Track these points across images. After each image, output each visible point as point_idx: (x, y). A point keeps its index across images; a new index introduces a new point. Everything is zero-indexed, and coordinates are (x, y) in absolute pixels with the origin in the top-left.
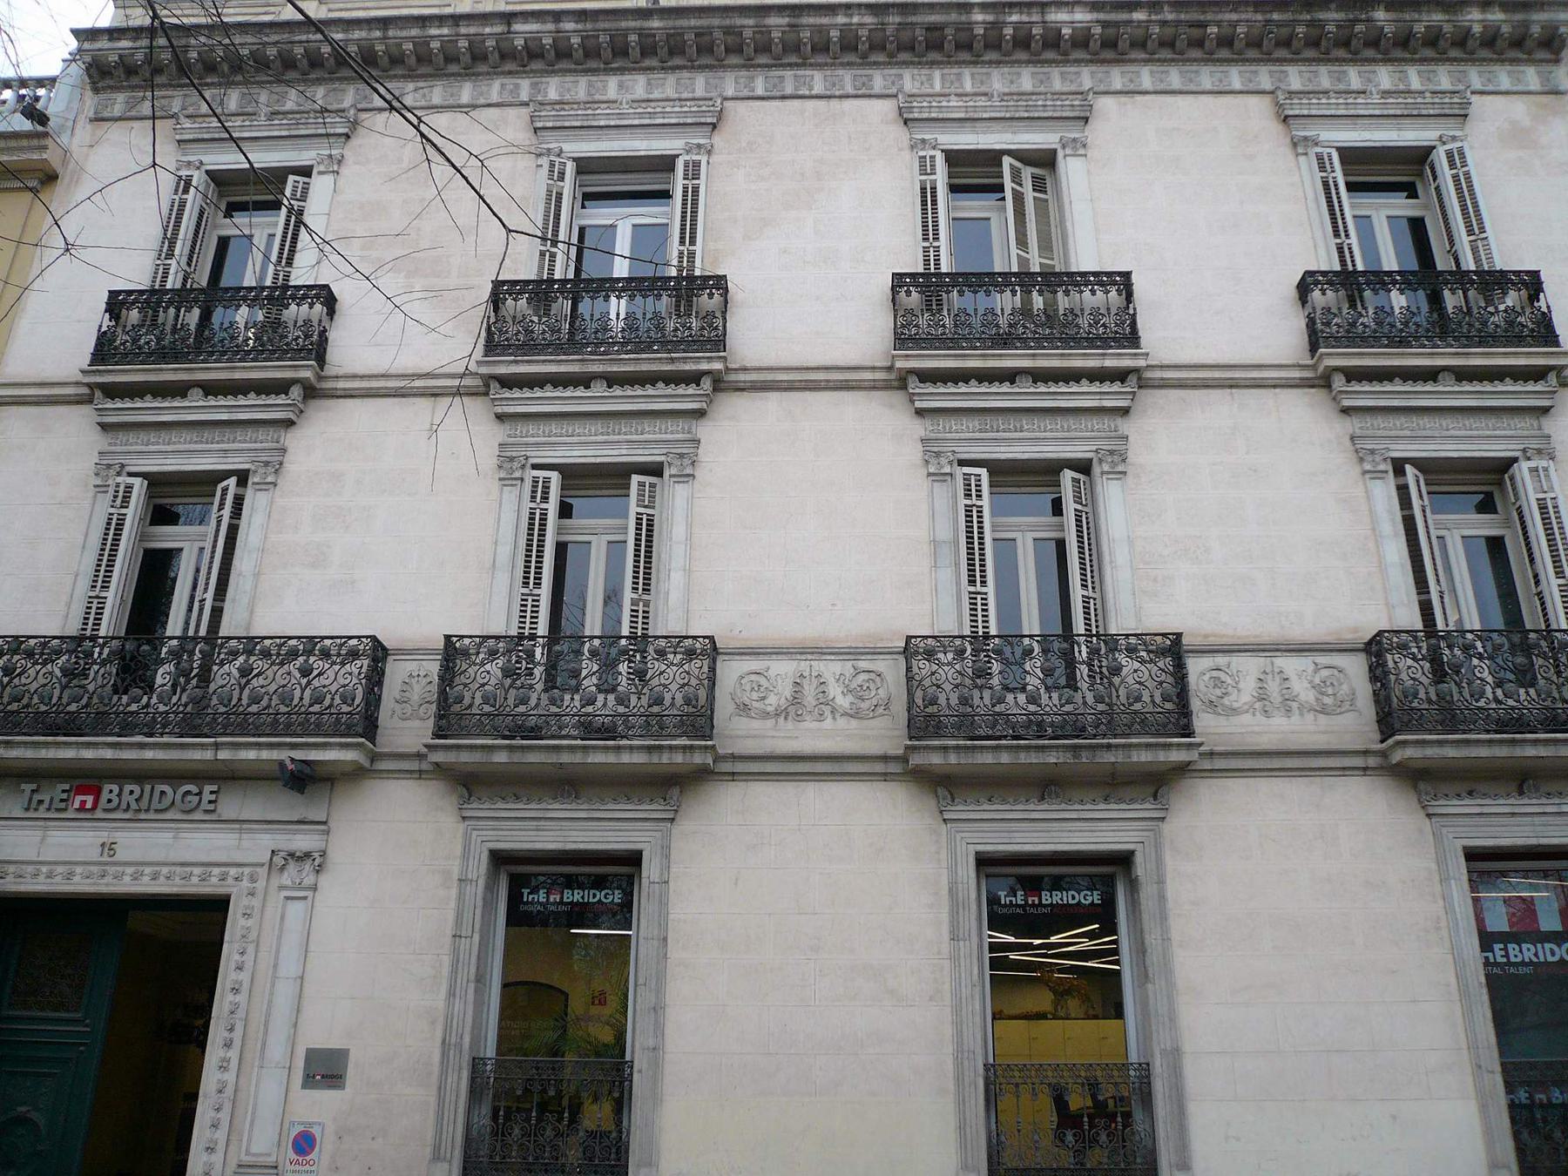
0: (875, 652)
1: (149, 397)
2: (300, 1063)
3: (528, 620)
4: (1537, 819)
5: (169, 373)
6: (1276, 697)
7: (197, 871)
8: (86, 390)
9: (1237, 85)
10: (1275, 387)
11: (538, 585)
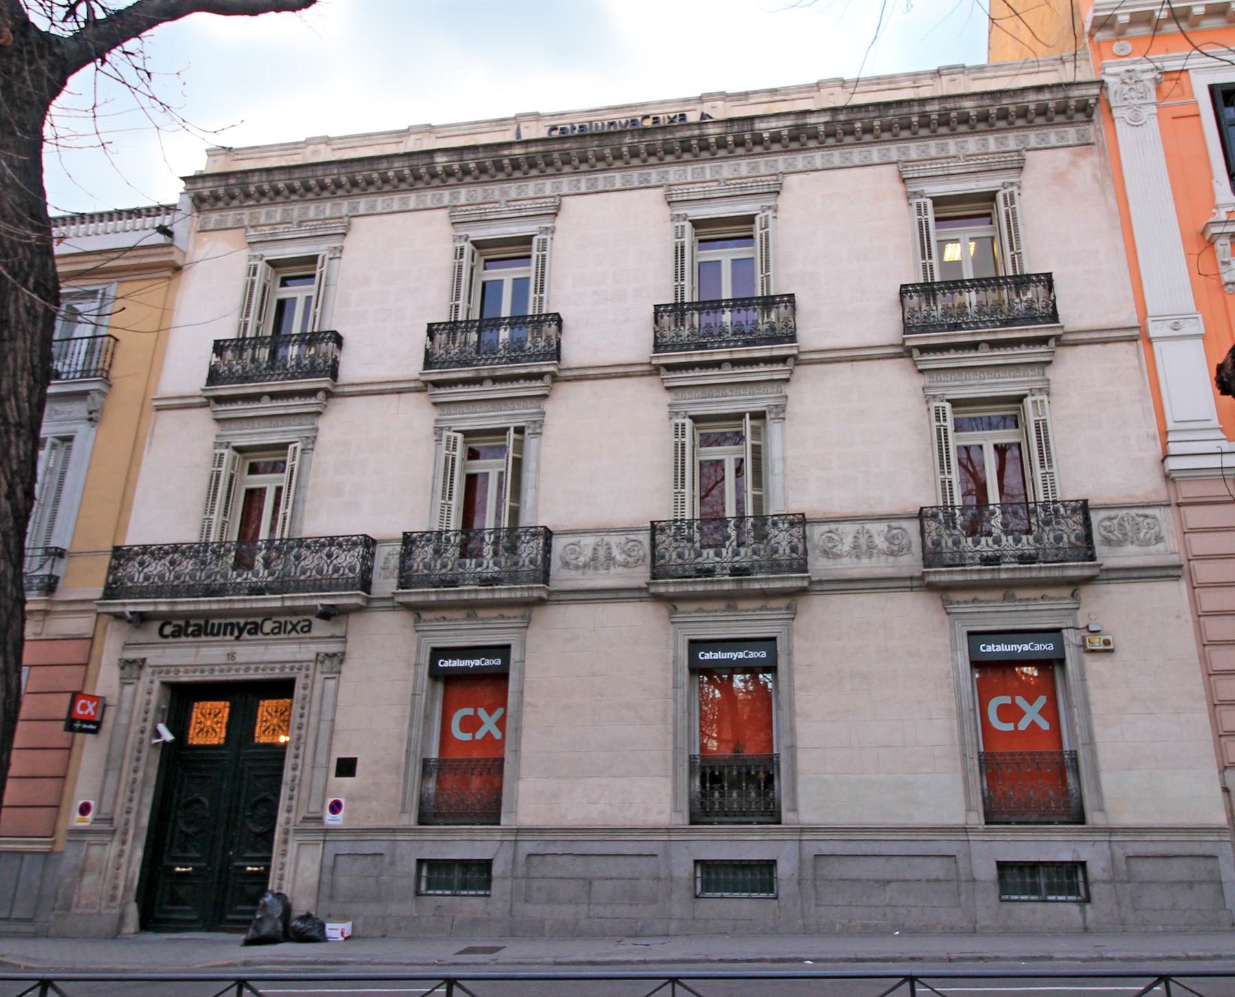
0: (638, 530)
2: (334, 765)
3: (679, 511)
4: (1013, 614)
5: (250, 388)
6: (864, 547)
7: (278, 666)
8: (204, 400)
9: (876, 159)
10: (879, 359)
11: (683, 486)
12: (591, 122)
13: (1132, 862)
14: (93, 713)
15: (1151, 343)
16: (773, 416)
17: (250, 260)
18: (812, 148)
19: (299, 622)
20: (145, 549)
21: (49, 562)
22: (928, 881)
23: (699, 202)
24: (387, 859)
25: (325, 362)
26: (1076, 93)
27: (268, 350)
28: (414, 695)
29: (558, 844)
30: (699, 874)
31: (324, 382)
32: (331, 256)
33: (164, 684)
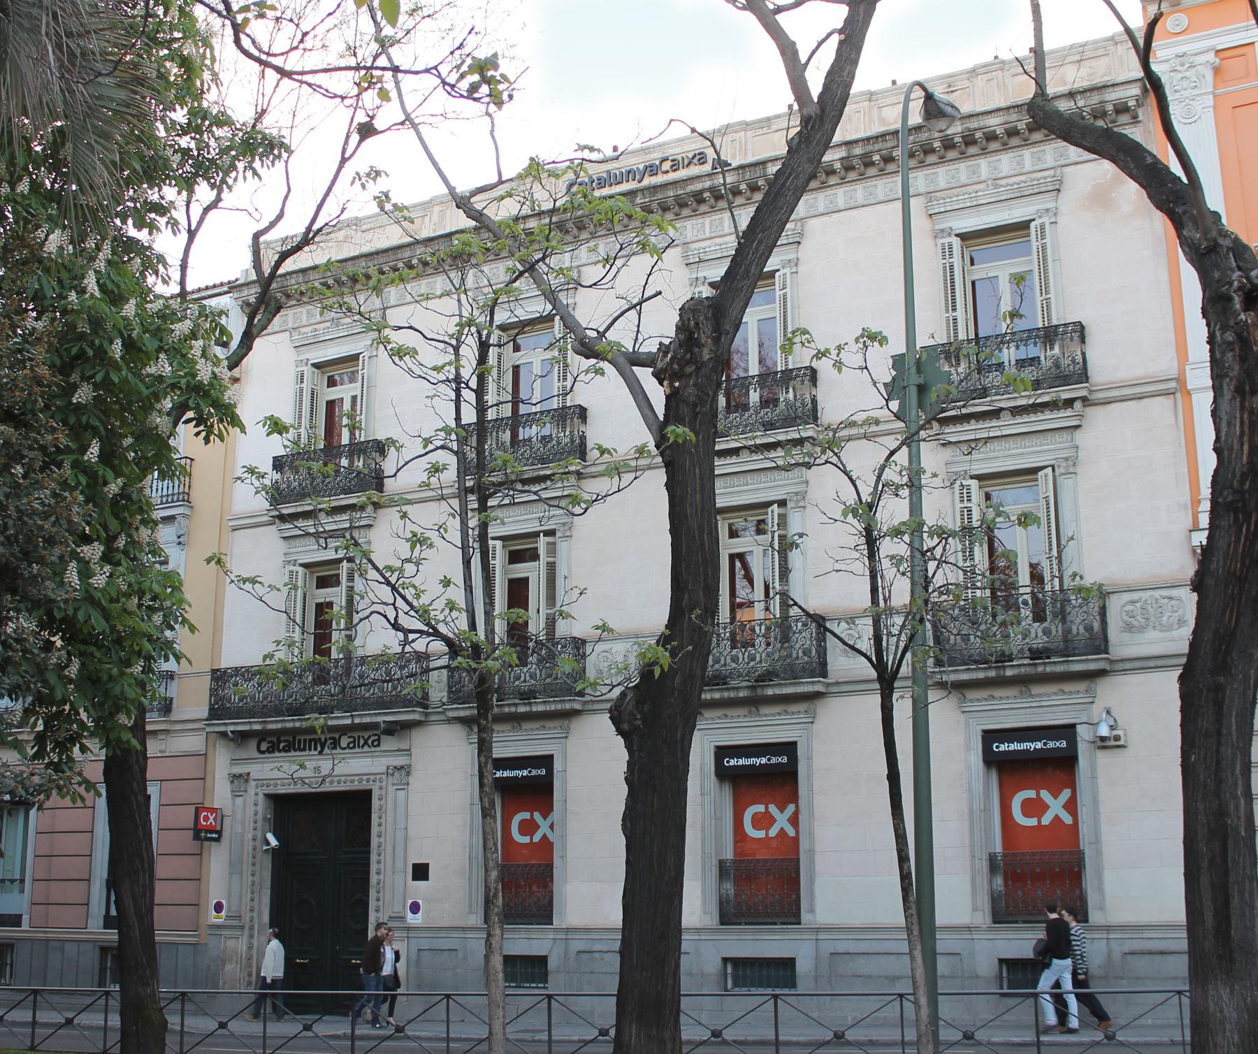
7: (357, 778)
12: (609, 172)
13: (1129, 957)
15: (1190, 395)
16: (793, 505)
18: (833, 185)
19: (369, 737)
20: (237, 670)
21: (164, 684)
24: (460, 955)
26: (1112, 96)
29: (603, 942)
30: (1005, 974)
33: (267, 796)
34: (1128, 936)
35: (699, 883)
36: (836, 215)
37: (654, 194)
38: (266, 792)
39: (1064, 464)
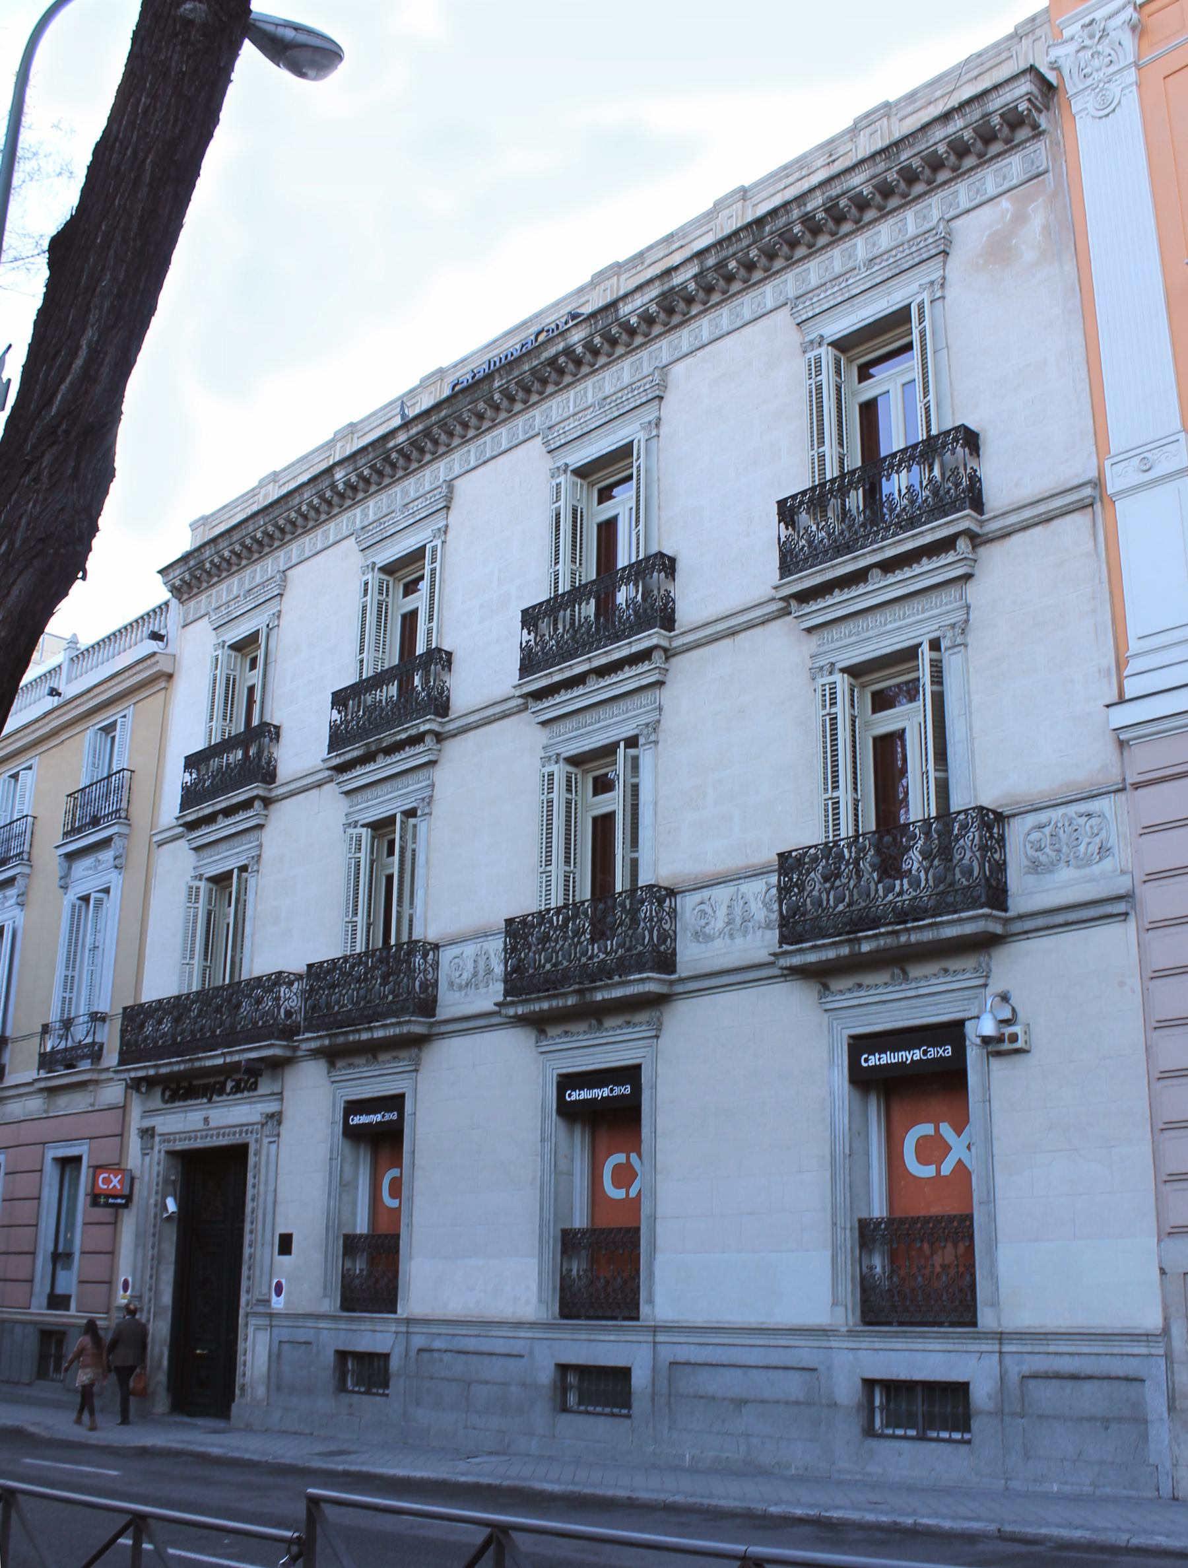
1: (925, 560)
5: (844, 566)
6: (738, 920)
8: (782, 604)
13: (1032, 1384)
14: (119, 1187)
17: (804, 352)
22: (787, 1403)
23: (882, 288)
25: (957, 485)
26: (996, 103)
27: (861, 491)
28: (331, 1159)
31: (963, 520)
32: (647, 437)
34: (1029, 1349)
35: (536, 1261)
36: (700, 353)
37: (509, 373)
38: (167, 1149)
39: (949, 634)
